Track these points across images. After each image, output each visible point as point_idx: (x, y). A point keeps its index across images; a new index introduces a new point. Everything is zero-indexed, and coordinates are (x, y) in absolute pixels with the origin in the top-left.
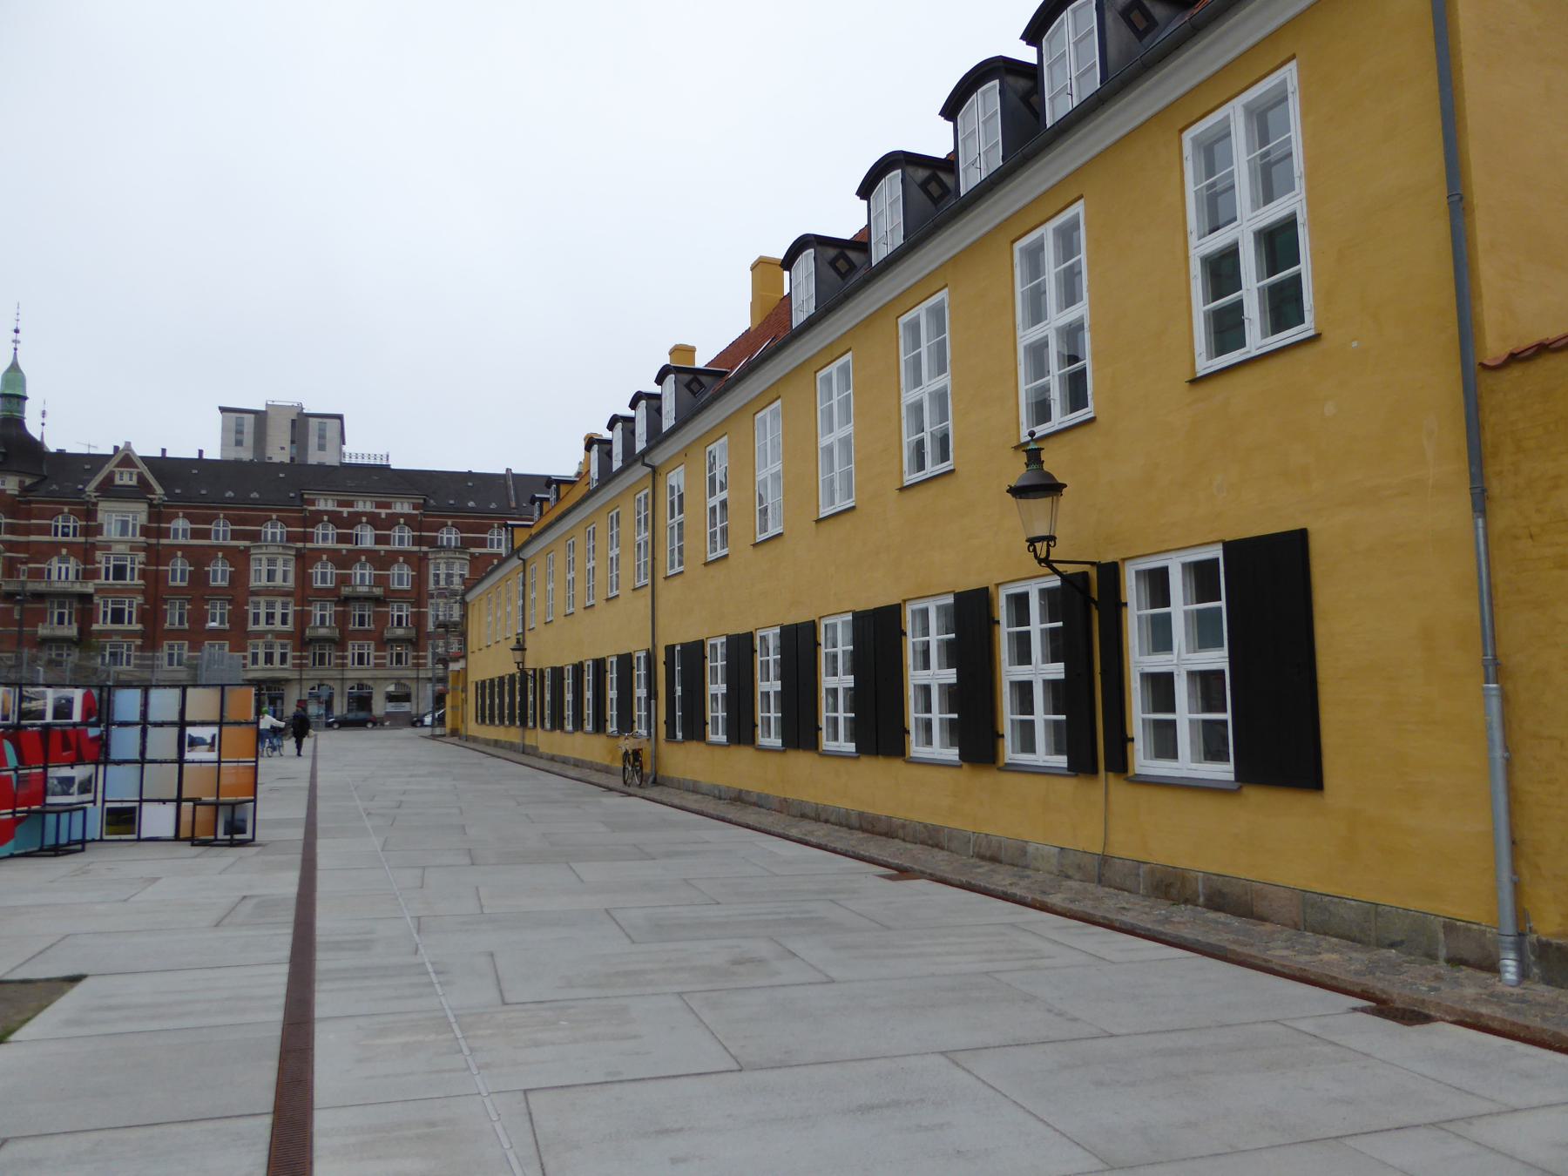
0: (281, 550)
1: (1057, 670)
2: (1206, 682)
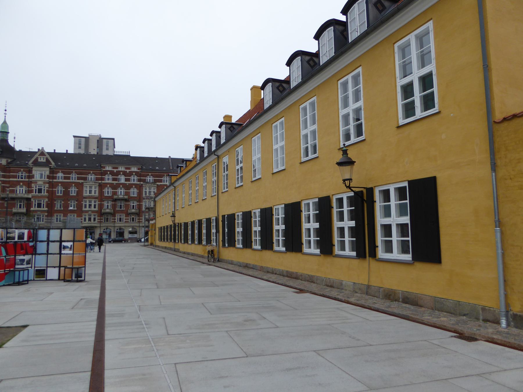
0: (94, 183)
1: (353, 223)
2: (402, 227)
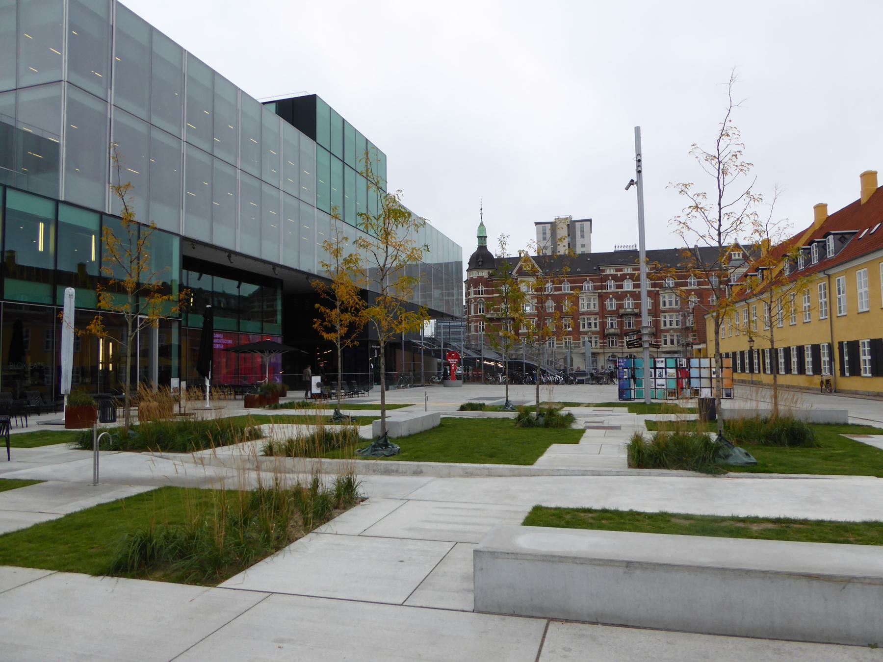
0: (592, 294)
